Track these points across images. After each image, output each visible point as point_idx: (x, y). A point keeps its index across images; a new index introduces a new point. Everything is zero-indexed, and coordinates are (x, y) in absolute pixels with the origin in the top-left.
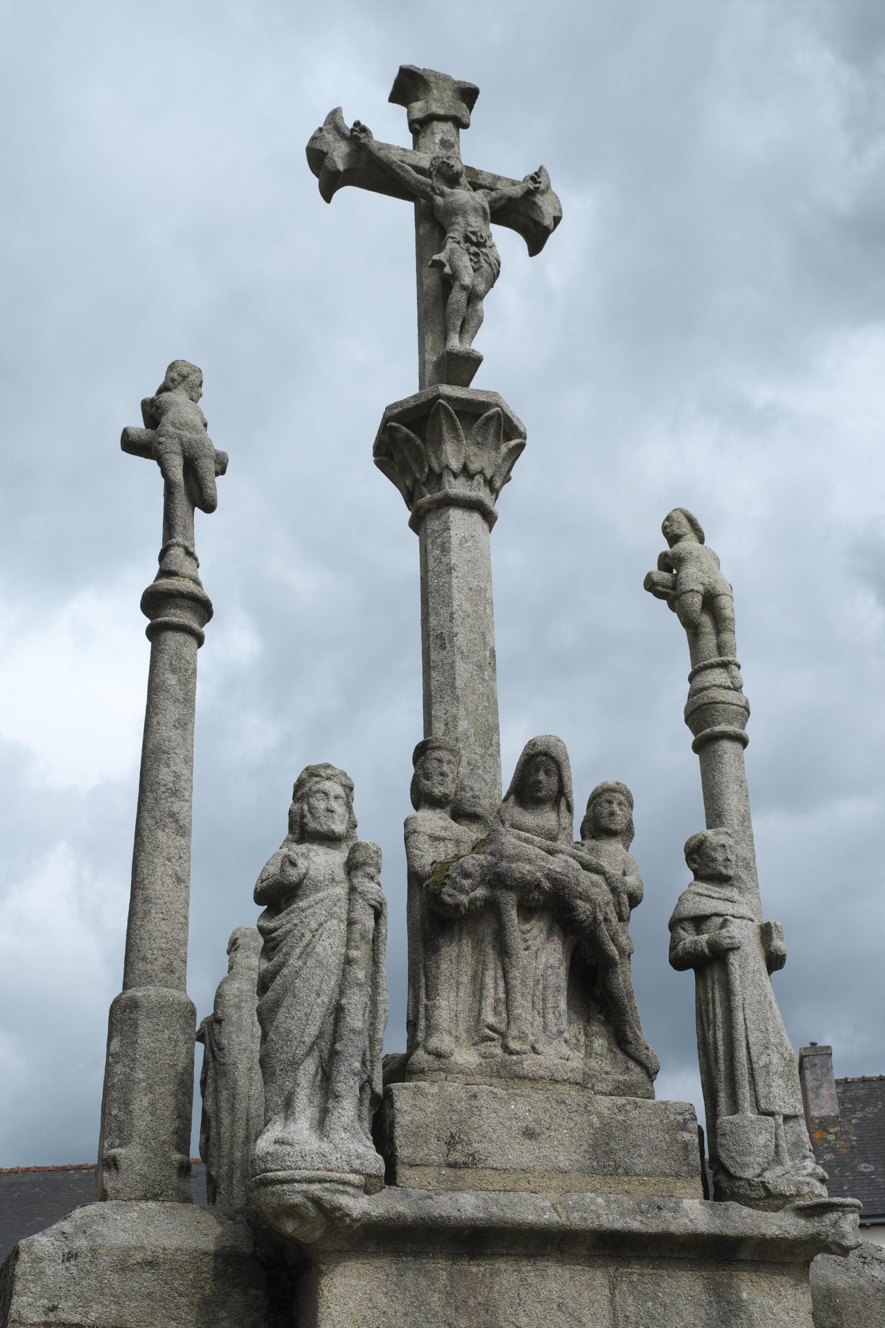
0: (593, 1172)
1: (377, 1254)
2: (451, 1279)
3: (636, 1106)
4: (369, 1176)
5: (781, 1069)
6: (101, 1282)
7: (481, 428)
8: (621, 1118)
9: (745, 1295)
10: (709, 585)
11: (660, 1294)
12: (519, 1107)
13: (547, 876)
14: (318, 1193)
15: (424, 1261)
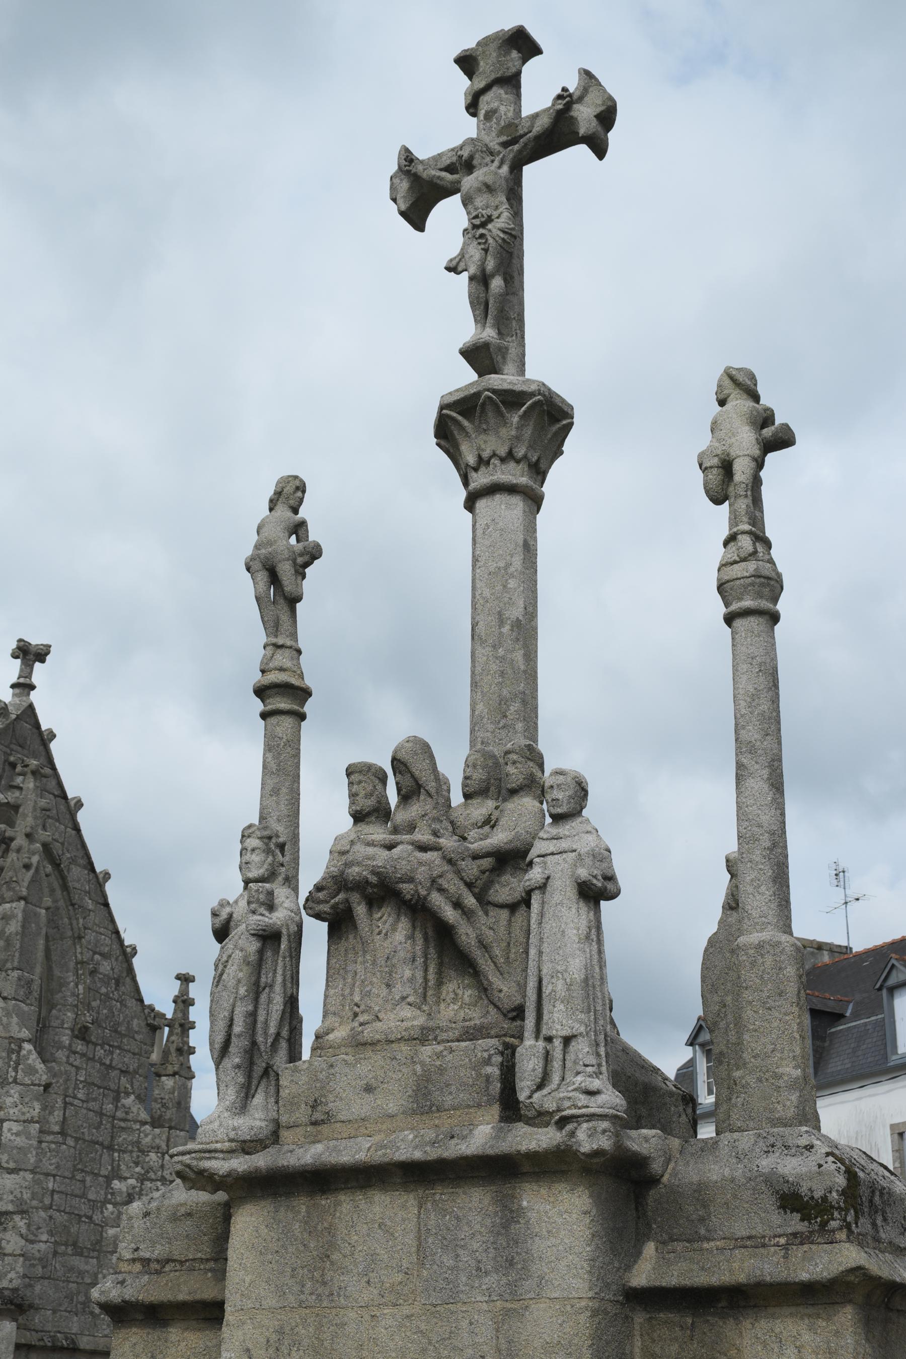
0: (414, 1112)
1: (263, 1197)
2: (308, 1212)
3: (451, 1051)
4: (244, 1142)
5: (563, 994)
6: (161, 1230)
7: (480, 417)
8: (438, 1063)
9: (525, 1203)
10: (723, 454)
11: (455, 1209)
12: (363, 1068)
13: (373, 873)
14: (188, 1162)
15: (292, 1199)
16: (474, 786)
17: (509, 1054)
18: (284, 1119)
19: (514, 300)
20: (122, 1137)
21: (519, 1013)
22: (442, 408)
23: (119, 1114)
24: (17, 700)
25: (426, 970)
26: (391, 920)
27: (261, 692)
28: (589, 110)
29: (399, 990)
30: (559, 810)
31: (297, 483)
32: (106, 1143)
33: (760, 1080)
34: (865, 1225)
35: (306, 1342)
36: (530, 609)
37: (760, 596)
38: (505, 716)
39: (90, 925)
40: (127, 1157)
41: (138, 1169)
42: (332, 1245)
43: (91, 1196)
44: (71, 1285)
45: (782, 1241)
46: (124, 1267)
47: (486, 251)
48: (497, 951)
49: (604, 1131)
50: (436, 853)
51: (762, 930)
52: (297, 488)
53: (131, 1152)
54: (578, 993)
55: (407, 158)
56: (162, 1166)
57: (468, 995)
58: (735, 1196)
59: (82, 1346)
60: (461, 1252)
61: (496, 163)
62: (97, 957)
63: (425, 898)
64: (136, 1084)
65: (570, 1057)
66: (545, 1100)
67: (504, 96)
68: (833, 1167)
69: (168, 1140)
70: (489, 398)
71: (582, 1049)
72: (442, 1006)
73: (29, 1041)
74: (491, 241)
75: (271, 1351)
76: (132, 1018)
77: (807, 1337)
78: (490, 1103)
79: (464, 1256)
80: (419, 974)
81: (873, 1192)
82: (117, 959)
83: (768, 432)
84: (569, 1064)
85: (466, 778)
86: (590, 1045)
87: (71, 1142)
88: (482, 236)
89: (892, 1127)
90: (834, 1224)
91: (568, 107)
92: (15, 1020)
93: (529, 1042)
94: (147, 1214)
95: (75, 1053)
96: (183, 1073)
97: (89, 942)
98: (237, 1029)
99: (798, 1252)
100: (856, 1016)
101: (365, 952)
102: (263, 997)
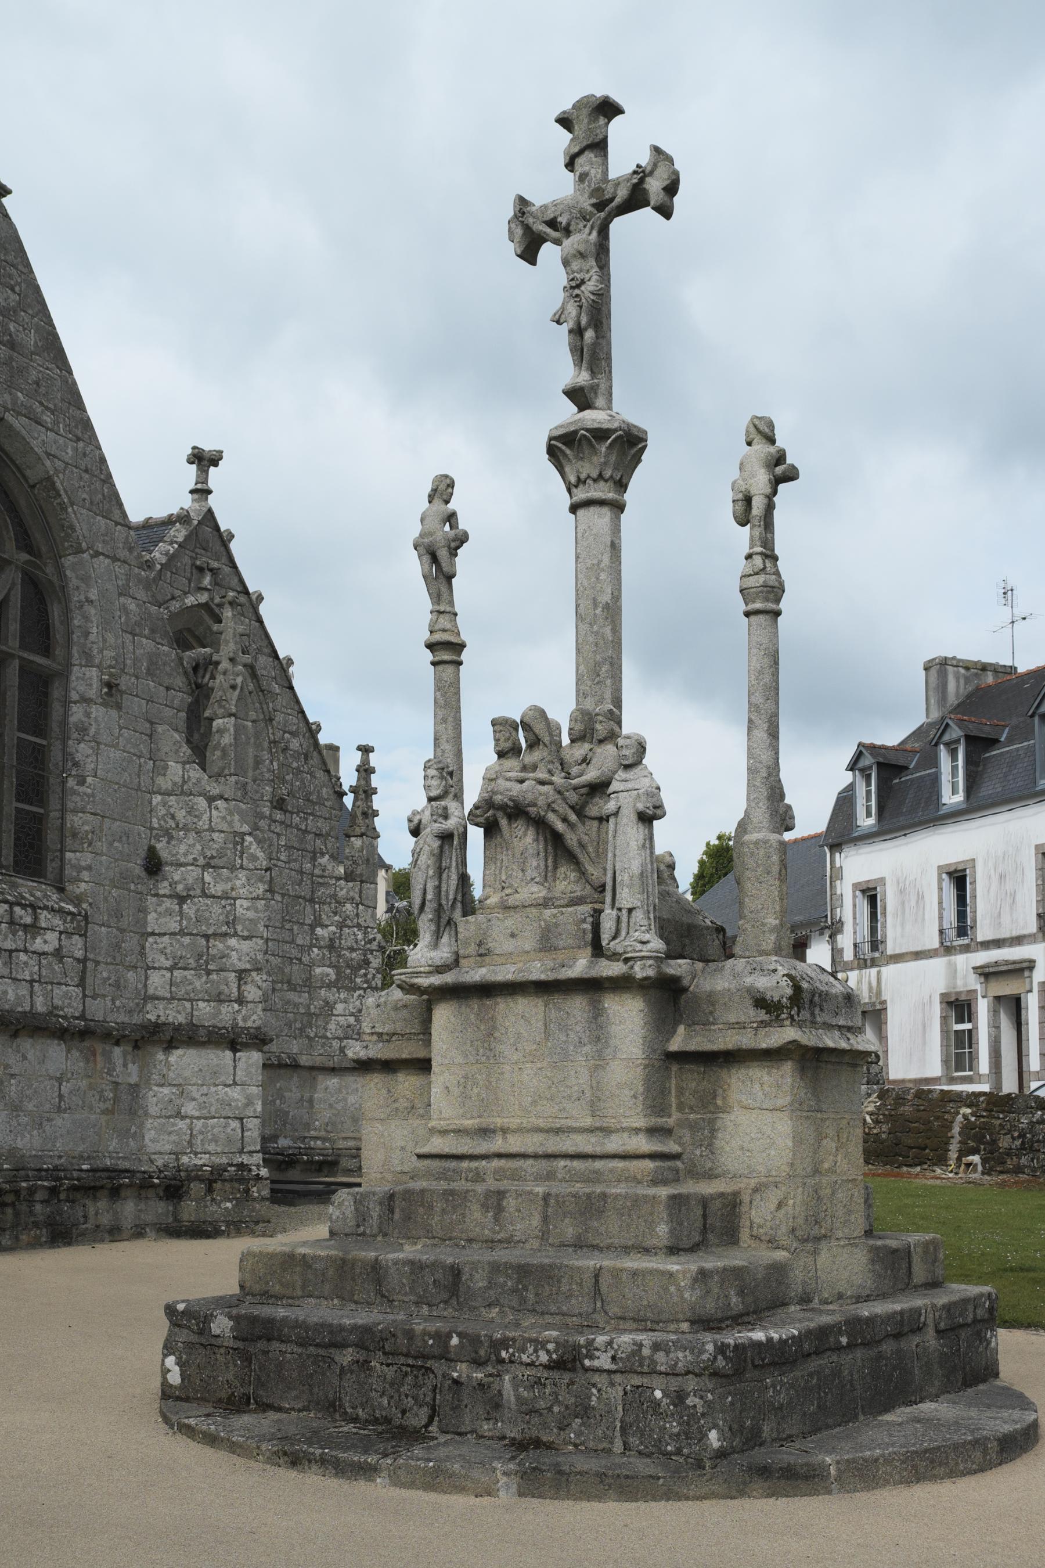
0: (541, 950)
1: (451, 999)
4: (438, 966)
12: (509, 923)
13: (510, 800)
16: (577, 734)
17: (597, 913)
18: (461, 952)
19: (603, 342)
20: (321, 892)
21: (602, 888)
22: (551, 439)
23: (317, 871)
24: (197, 505)
25: (546, 860)
26: (523, 829)
27: (430, 646)
28: (658, 183)
29: (530, 873)
30: (626, 762)
31: (448, 481)
32: (308, 897)
33: (753, 926)
34: (805, 1014)
35: (481, 1083)
36: (616, 594)
37: (767, 600)
38: (599, 675)
39: (278, 708)
40: (326, 907)
41: (337, 918)
42: (494, 1028)
43: (299, 942)
44: (289, 1015)
45: (755, 1025)
46: (367, 1038)
47: (581, 307)
48: (590, 849)
49: (650, 966)
50: (550, 787)
51: (759, 832)
52: (448, 486)
53: (330, 903)
54: (637, 881)
55: (522, 202)
56: (357, 915)
57: (573, 875)
58: (730, 1000)
59: (302, 1064)
60: (570, 1032)
61: (587, 230)
62: (287, 735)
63: (544, 816)
64: (329, 845)
65: (632, 920)
66: (617, 946)
67: (594, 159)
68: (785, 983)
69: (361, 892)
70: (584, 436)
71: (639, 916)
72: (558, 882)
73: (250, 834)
74: (584, 300)
75: (461, 1088)
76: (321, 787)
77: (766, 1078)
78: (585, 946)
79: (572, 1035)
80: (542, 864)
81: (813, 995)
82: (304, 736)
83: (779, 470)
84: (631, 924)
85: (570, 729)
86: (644, 914)
87: (278, 898)
88: (577, 296)
89: (1037, 847)
90: (784, 1016)
91: (642, 181)
92: (237, 817)
93: (608, 911)
94: (378, 1006)
95: (275, 821)
96: (369, 833)
97: (279, 723)
98: (430, 896)
99: (762, 1032)
100: (1010, 741)
101: (507, 849)
102: (444, 876)
